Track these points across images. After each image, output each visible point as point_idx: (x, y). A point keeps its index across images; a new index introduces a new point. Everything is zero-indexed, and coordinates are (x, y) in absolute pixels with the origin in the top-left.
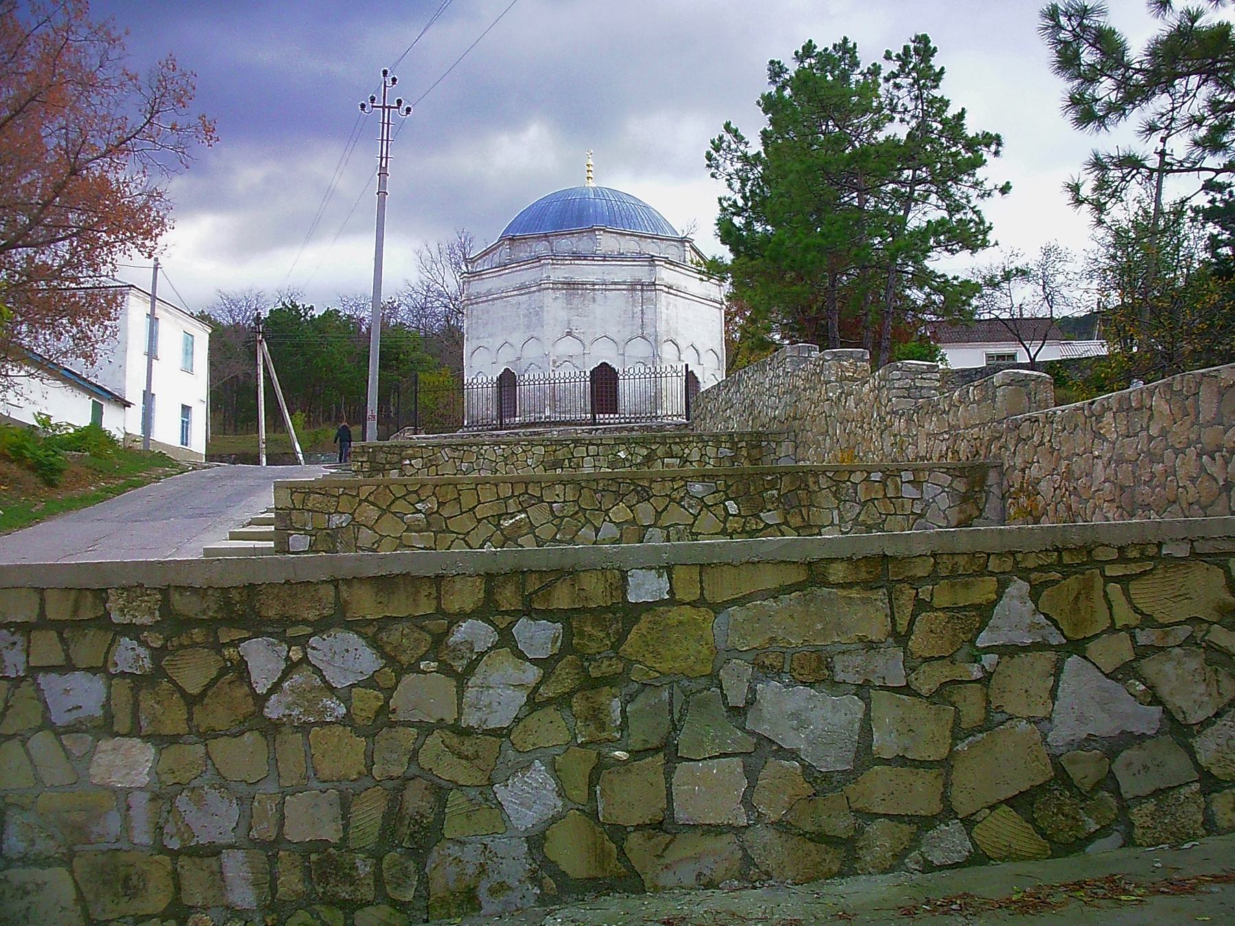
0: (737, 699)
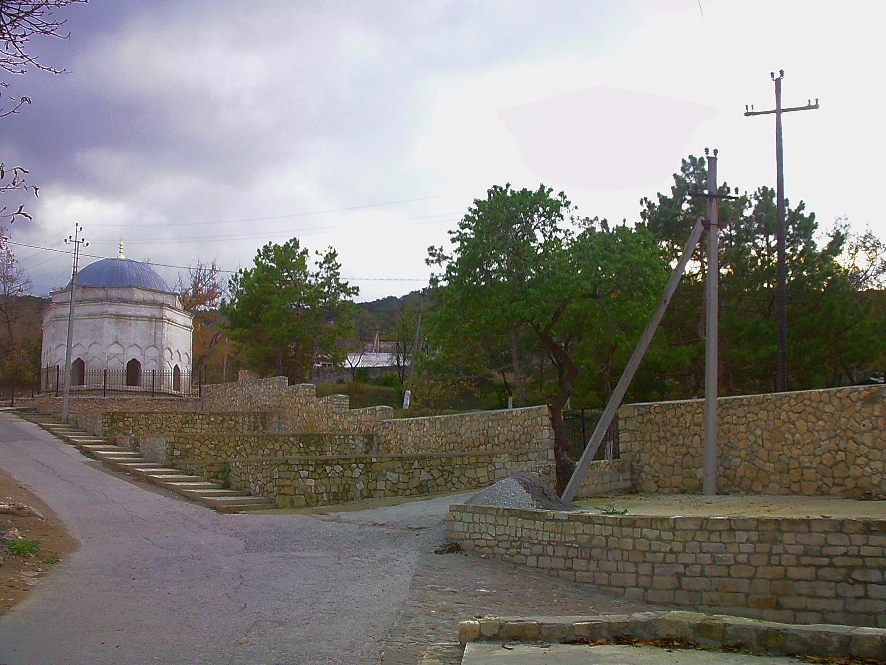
0: (384, 474)
